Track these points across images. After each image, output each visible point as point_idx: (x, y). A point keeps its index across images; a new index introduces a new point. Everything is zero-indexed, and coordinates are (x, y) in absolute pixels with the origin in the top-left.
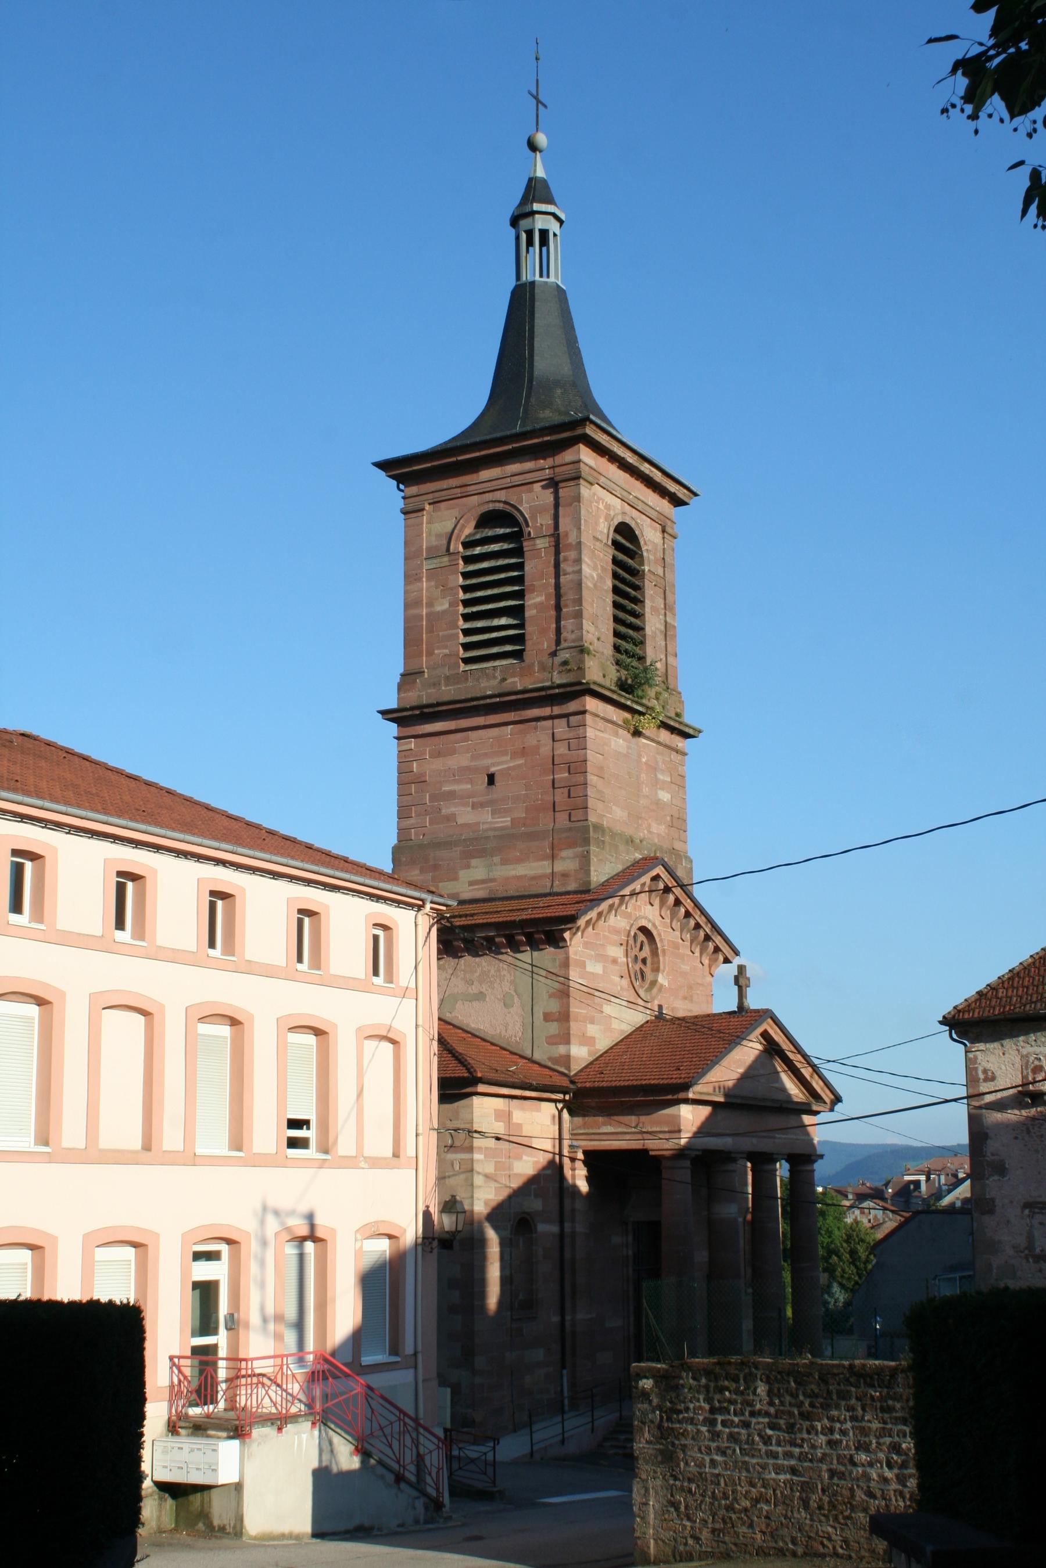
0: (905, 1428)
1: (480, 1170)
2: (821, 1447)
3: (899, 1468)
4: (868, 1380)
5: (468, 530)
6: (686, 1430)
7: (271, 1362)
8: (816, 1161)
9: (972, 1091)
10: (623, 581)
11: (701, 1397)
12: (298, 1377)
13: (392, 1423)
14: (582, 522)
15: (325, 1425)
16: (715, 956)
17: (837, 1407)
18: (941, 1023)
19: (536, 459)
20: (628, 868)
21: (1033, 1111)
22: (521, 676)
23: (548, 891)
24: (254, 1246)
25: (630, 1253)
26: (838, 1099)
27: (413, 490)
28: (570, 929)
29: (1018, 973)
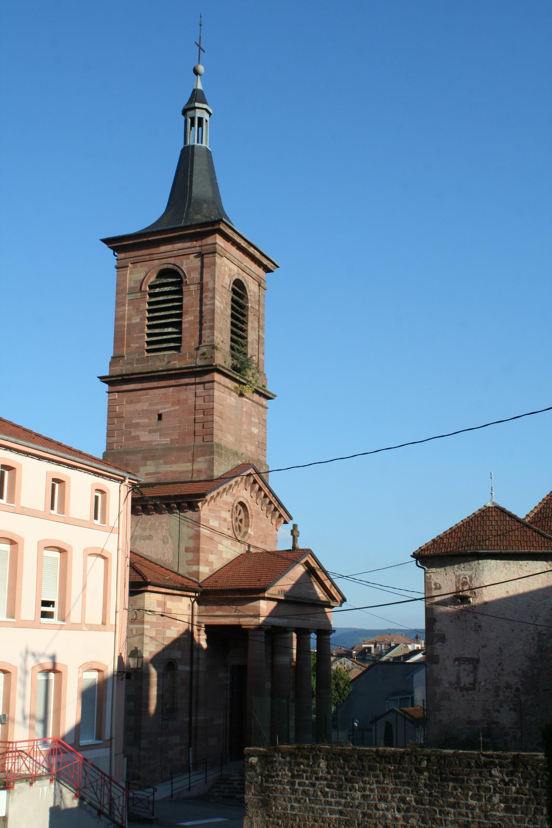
0: (408, 788)
1: (148, 634)
2: (358, 799)
3: (404, 812)
4: (387, 759)
5: (152, 279)
6: (276, 788)
7: (26, 744)
8: (331, 634)
9: (427, 595)
10: (237, 311)
11: (286, 768)
12: (43, 753)
13: (97, 780)
14: (216, 277)
15: (58, 781)
16: (279, 519)
17: (368, 775)
18: (412, 556)
19: (192, 241)
20: (234, 469)
21: (461, 607)
22: (179, 360)
23: (189, 480)
24: (20, 674)
25: (229, 683)
26: (344, 600)
27: (122, 255)
28: (201, 501)
29: (455, 530)
